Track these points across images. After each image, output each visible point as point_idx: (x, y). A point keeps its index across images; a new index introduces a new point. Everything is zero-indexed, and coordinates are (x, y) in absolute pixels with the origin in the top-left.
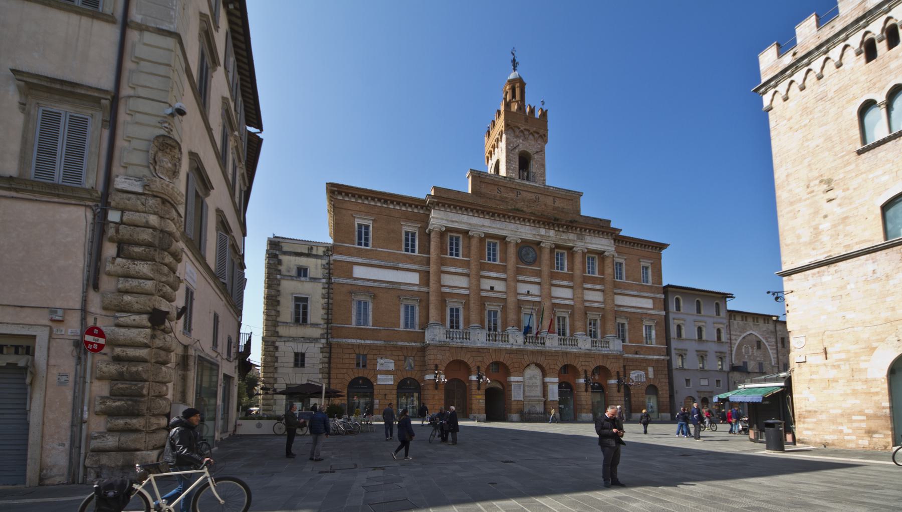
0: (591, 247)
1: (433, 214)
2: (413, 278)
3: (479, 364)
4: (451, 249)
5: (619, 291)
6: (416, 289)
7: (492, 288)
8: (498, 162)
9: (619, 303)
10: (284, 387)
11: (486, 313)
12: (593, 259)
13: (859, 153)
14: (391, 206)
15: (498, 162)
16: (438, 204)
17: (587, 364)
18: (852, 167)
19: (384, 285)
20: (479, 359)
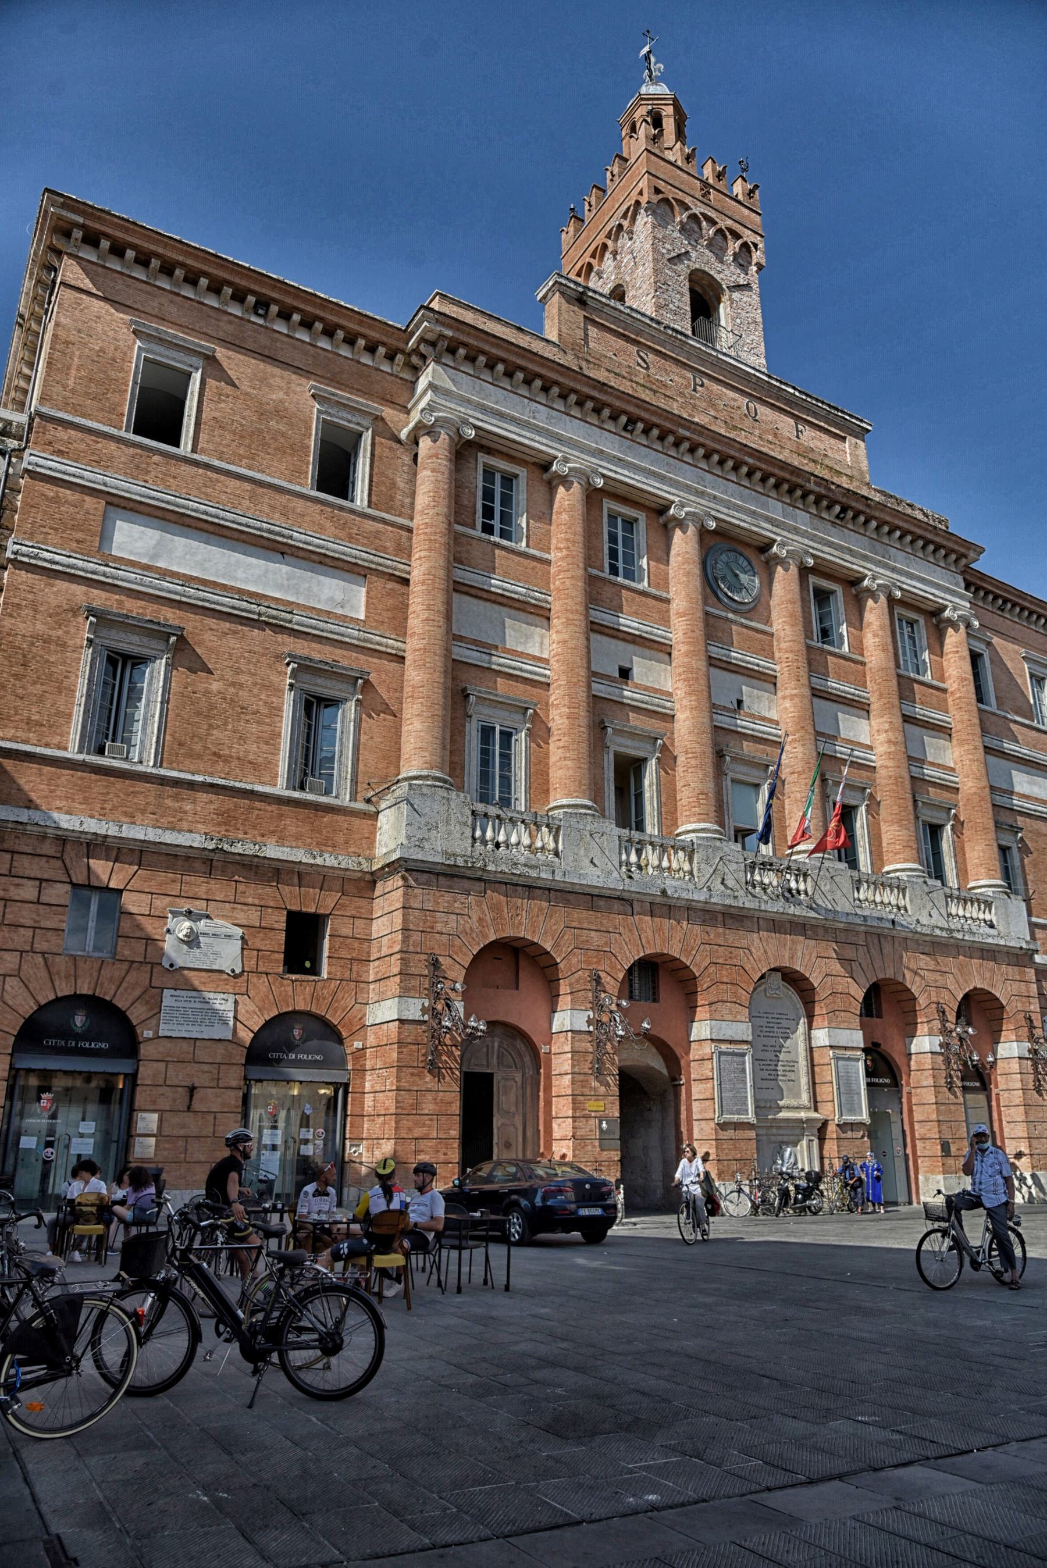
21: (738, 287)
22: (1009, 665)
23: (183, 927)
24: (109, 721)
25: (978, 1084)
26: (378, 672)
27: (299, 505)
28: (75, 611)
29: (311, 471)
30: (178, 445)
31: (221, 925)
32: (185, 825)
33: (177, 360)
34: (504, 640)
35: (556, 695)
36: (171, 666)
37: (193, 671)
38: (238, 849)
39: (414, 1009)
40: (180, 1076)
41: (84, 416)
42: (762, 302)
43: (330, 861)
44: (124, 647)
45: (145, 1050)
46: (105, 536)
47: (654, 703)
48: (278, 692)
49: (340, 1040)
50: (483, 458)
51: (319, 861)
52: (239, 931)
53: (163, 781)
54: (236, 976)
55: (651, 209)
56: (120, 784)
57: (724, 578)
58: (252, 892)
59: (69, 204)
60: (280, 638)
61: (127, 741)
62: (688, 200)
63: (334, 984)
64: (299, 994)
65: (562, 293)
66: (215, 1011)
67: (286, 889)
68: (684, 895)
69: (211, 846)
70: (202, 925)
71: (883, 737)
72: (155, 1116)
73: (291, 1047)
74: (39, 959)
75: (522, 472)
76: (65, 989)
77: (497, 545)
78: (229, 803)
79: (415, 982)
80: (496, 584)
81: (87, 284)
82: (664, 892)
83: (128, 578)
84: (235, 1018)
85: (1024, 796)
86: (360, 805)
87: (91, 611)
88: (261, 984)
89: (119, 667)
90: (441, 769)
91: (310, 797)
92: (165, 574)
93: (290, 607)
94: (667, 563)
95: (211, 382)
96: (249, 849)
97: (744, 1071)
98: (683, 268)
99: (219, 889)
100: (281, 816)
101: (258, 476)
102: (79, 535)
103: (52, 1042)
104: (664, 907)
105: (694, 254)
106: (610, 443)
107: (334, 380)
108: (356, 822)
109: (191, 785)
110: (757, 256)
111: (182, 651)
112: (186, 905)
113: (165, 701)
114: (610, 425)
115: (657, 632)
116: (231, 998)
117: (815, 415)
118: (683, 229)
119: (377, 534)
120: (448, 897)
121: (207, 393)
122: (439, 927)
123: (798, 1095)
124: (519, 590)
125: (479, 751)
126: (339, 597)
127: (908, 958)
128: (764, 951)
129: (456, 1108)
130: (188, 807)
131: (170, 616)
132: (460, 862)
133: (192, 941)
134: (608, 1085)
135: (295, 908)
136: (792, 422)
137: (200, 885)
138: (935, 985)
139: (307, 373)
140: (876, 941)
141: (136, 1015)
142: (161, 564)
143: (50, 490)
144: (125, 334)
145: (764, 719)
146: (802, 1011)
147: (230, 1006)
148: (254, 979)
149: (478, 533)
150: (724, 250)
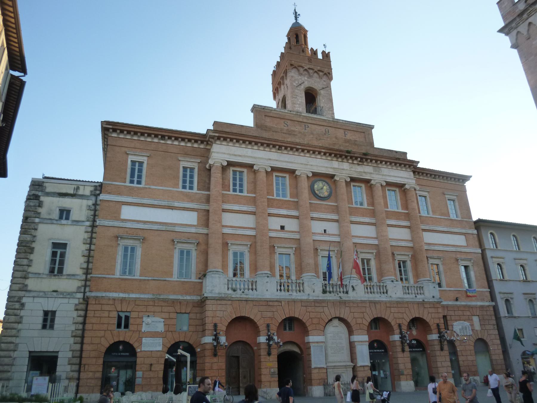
2: (190, 218)
6: (193, 230)
7: (282, 228)
19: (155, 227)
25: (421, 349)
40: (148, 361)
41: (115, 181)
45: (138, 355)
50: (232, 169)
52: (163, 320)
74: (109, 332)
75: (245, 170)
76: (116, 340)
103: (114, 354)
122: (218, 315)
129: (224, 367)
140: (374, 305)
141: (135, 346)
149: (231, 192)
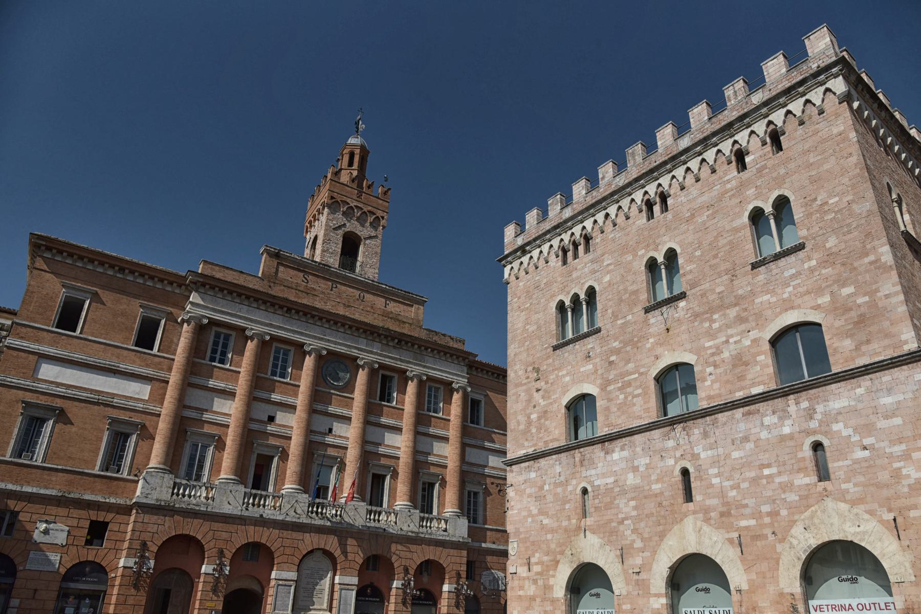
0: (432, 373)
1: (194, 297)
3: (221, 545)
4: (214, 351)
5: (473, 442)
8: (316, 238)
9: (473, 461)
10: (798, 523)
11: (254, 458)
12: (437, 389)
13: (555, 348)
14: (130, 278)
15: (316, 238)
16: (203, 285)
17: (409, 555)
18: (551, 361)
20: (225, 535)
21: (370, 238)
22: (497, 405)
23: (43, 526)
24: (27, 443)
26: (148, 421)
27: (125, 353)
28: (17, 402)
29: (133, 338)
30: (74, 331)
31: (60, 526)
32: (51, 486)
33: (79, 296)
34: (212, 407)
35: (231, 431)
36: (55, 423)
37: (65, 424)
38: (72, 496)
39: (131, 562)
41: (35, 322)
42: (382, 244)
43: (113, 500)
44: (37, 415)
45: (18, 574)
46: (36, 370)
47: (282, 431)
48: (102, 431)
49: (106, 573)
50: (215, 329)
51: (107, 500)
52: (67, 528)
53: (44, 468)
54: (63, 546)
55: (329, 207)
56: (25, 470)
57: (330, 375)
58: (75, 513)
59: (40, 237)
60: (106, 409)
61: (33, 453)
62: (348, 200)
63: (106, 550)
64: (90, 554)
65: (268, 253)
66: (49, 560)
67: (91, 512)
68: (272, 517)
69: (60, 494)
70: (52, 526)
71: (404, 444)
72: (18, 601)
73: (85, 576)
77: (215, 366)
78: (71, 477)
79: (134, 551)
80: (212, 383)
81: (45, 267)
82: (261, 516)
83: (42, 387)
84: (60, 563)
85: (493, 468)
86: (131, 478)
87: (23, 402)
88: (73, 550)
89: (32, 427)
90: (164, 464)
91: (109, 474)
92: (58, 385)
93: (114, 396)
94: (302, 370)
95: (94, 304)
96: (77, 496)
97: (289, 593)
98: (341, 232)
99: (62, 511)
100: (94, 482)
101: (108, 342)
102: (24, 371)
104: (262, 522)
105: (348, 225)
106: (277, 320)
107: (152, 299)
108: (129, 484)
109: (57, 470)
110: (383, 222)
111: (62, 416)
112: (46, 518)
113: (51, 436)
114: (279, 312)
115: (290, 400)
116: (59, 555)
117: (397, 296)
118: (344, 213)
119: (160, 363)
120: (156, 517)
121: (91, 308)
122: (149, 530)
123: (322, 604)
124: (221, 385)
125: (185, 454)
126: (138, 390)
127: (394, 547)
128: (310, 541)
130: (54, 479)
131: (58, 403)
132: (163, 503)
133: (46, 532)
134: (218, 596)
135: (94, 519)
136: (383, 300)
137: (53, 510)
138: (406, 559)
139: (136, 296)
142: (58, 381)
143: (15, 353)
144: (59, 286)
145: (340, 437)
146: (331, 567)
147: (58, 558)
148: (71, 547)
150: (366, 221)
